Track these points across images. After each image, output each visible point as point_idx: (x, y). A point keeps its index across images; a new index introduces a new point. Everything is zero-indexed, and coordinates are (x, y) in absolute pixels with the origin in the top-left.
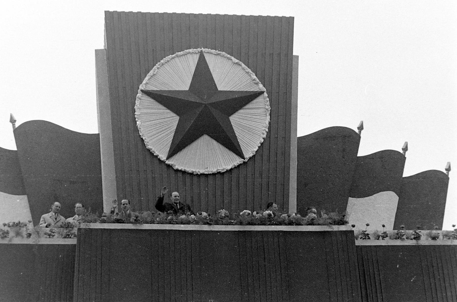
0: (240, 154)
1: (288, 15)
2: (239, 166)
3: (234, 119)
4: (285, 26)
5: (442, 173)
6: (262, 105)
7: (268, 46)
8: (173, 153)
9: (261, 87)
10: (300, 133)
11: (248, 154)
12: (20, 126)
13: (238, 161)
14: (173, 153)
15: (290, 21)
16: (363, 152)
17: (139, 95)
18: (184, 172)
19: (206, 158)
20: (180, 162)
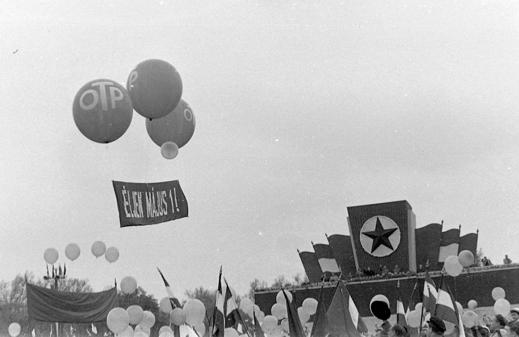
1: (174, 179)
3: (389, 238)
5: (451, 309)
6: (398, 232)
7: (399, 211)
8: (373, 250)
11: (395, 249)
14: (373, 250)
16: (444, 230)
18: (377, 257)
19: (383, 251)
20: (375, 254)
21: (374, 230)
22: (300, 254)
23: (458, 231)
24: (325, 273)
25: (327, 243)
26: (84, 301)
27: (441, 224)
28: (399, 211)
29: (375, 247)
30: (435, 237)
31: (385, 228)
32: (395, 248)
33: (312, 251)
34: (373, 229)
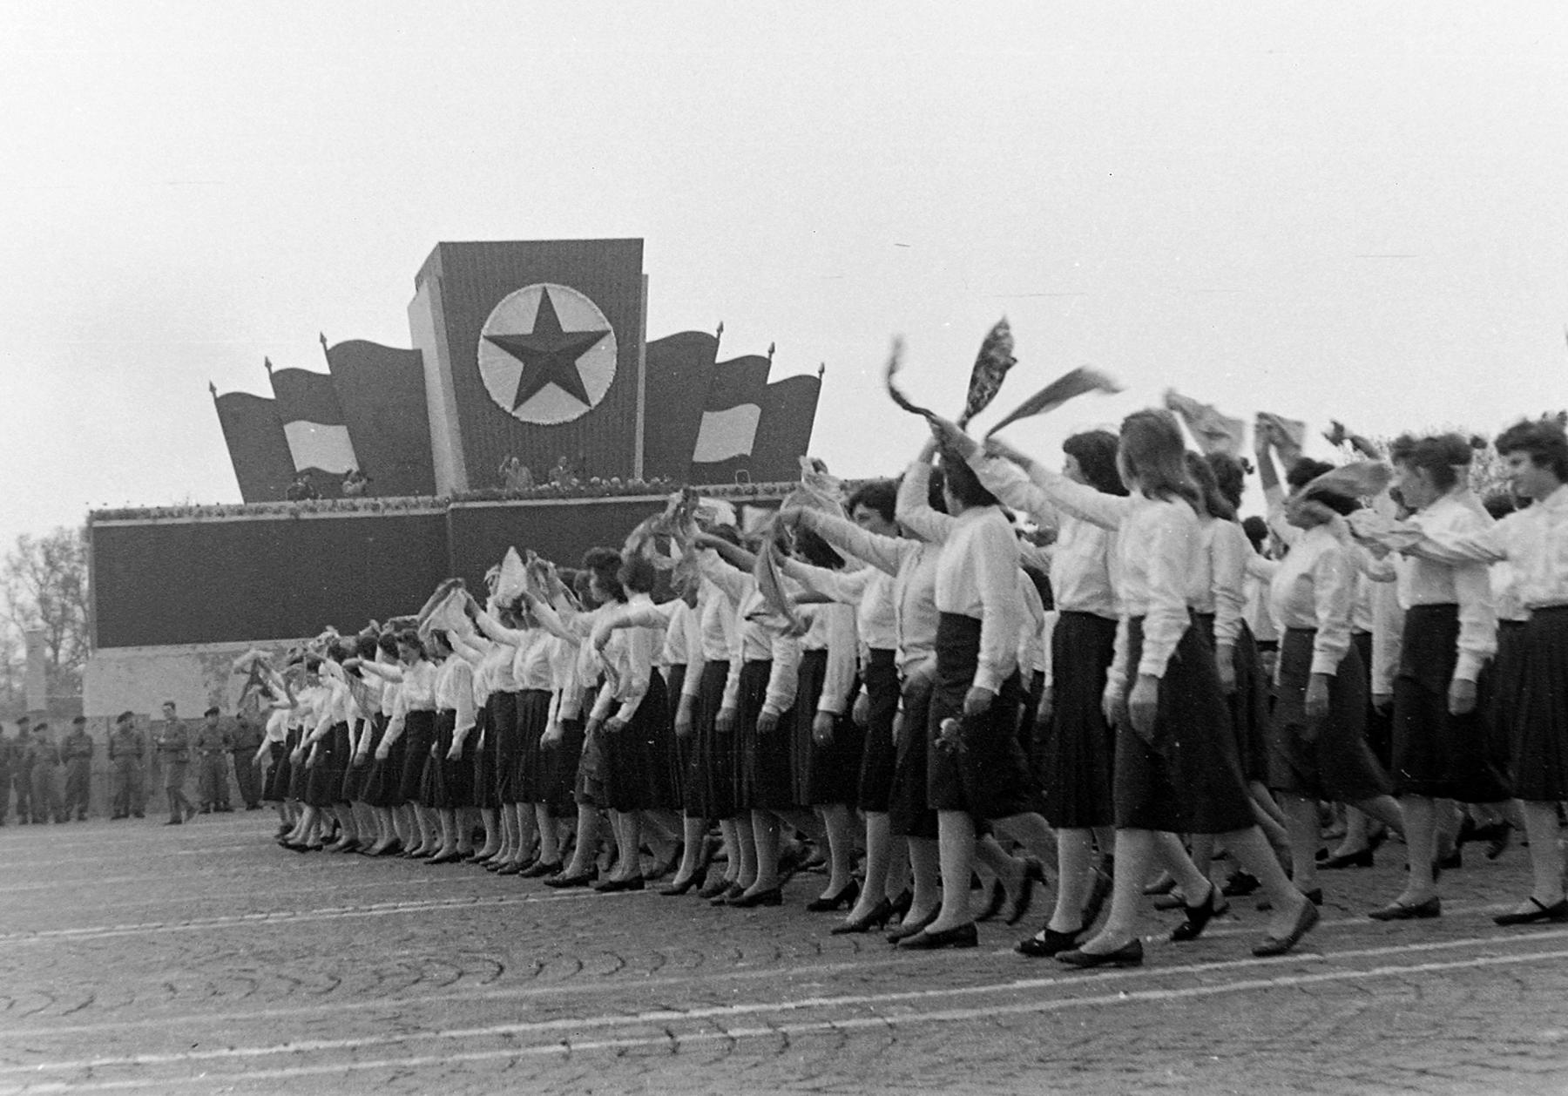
0: (585, 400)
2: (585, 415)
4: (634, 248)
7: (612, 270)
8: (519, 402)
9: (608, 326)
10: (649, 339)
11: (595, 402)
12: (334, 348)
13: (585, 409)
14: (519, 402)
15: (640, 242)
16: (721, 358)
17: (482, 341)
19: (553, 408)
20: (527, 414)
21: (530, 331)
22: (217, 400)
23: (763, 364)
24: (302, 473)
25: (323, 368)
26: (375, 742)
27: (715, 334)
28: (612, 270)
29: (526, 391)
30: (696, 374)
31: (566, 328)
32: (596, 397)
33: (268, 392)
34: (526, 326)
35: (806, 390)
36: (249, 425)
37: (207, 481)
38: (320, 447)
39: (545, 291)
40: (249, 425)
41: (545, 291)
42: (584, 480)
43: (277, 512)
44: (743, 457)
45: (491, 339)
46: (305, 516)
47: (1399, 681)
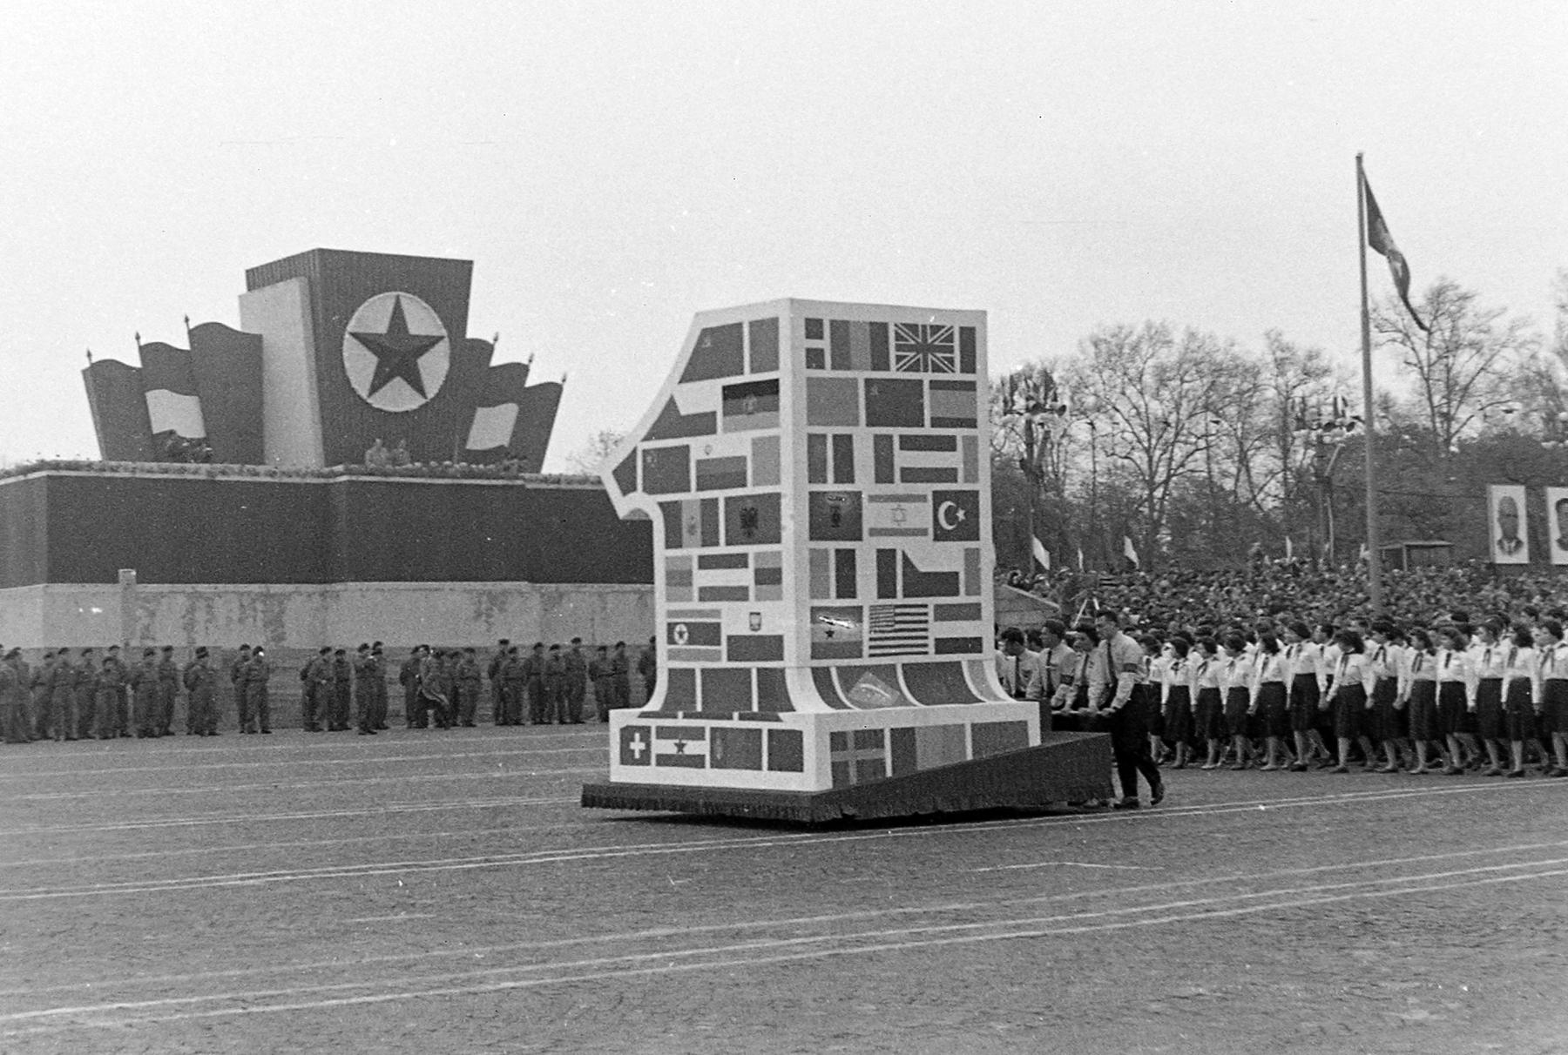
7: (446, 283)
9: (444, 332)
11: (431, 395)
13: (424, 401)
14: (374, 389)
16: (496, 361)
25: (183, 343)
28: (446, 283)
34: (382, 328)
35: (551, 394)
36: (114, 390)
37: (76, 439)
38: (175, 414)
39: (398, 298)
40: (114, 390)
41: (398, 298)
42: (426, 463)
43: (195, 472)
44: (501, 447)
45: (354, 335)
46: (220, 478)
47: (1478, 701)
